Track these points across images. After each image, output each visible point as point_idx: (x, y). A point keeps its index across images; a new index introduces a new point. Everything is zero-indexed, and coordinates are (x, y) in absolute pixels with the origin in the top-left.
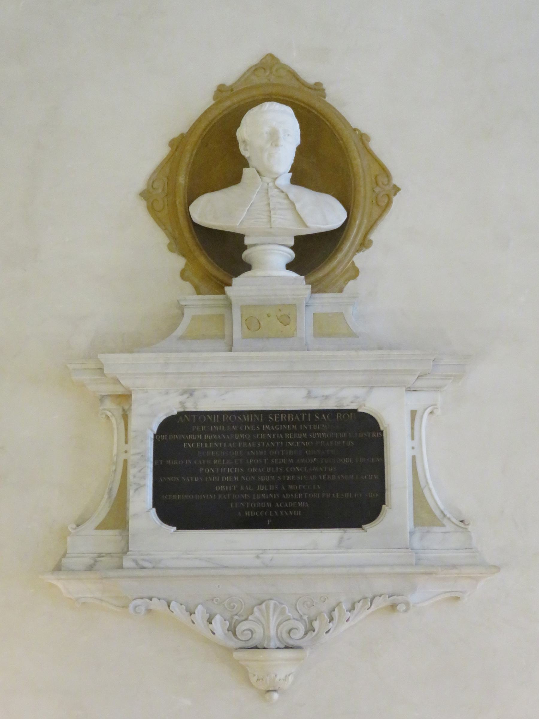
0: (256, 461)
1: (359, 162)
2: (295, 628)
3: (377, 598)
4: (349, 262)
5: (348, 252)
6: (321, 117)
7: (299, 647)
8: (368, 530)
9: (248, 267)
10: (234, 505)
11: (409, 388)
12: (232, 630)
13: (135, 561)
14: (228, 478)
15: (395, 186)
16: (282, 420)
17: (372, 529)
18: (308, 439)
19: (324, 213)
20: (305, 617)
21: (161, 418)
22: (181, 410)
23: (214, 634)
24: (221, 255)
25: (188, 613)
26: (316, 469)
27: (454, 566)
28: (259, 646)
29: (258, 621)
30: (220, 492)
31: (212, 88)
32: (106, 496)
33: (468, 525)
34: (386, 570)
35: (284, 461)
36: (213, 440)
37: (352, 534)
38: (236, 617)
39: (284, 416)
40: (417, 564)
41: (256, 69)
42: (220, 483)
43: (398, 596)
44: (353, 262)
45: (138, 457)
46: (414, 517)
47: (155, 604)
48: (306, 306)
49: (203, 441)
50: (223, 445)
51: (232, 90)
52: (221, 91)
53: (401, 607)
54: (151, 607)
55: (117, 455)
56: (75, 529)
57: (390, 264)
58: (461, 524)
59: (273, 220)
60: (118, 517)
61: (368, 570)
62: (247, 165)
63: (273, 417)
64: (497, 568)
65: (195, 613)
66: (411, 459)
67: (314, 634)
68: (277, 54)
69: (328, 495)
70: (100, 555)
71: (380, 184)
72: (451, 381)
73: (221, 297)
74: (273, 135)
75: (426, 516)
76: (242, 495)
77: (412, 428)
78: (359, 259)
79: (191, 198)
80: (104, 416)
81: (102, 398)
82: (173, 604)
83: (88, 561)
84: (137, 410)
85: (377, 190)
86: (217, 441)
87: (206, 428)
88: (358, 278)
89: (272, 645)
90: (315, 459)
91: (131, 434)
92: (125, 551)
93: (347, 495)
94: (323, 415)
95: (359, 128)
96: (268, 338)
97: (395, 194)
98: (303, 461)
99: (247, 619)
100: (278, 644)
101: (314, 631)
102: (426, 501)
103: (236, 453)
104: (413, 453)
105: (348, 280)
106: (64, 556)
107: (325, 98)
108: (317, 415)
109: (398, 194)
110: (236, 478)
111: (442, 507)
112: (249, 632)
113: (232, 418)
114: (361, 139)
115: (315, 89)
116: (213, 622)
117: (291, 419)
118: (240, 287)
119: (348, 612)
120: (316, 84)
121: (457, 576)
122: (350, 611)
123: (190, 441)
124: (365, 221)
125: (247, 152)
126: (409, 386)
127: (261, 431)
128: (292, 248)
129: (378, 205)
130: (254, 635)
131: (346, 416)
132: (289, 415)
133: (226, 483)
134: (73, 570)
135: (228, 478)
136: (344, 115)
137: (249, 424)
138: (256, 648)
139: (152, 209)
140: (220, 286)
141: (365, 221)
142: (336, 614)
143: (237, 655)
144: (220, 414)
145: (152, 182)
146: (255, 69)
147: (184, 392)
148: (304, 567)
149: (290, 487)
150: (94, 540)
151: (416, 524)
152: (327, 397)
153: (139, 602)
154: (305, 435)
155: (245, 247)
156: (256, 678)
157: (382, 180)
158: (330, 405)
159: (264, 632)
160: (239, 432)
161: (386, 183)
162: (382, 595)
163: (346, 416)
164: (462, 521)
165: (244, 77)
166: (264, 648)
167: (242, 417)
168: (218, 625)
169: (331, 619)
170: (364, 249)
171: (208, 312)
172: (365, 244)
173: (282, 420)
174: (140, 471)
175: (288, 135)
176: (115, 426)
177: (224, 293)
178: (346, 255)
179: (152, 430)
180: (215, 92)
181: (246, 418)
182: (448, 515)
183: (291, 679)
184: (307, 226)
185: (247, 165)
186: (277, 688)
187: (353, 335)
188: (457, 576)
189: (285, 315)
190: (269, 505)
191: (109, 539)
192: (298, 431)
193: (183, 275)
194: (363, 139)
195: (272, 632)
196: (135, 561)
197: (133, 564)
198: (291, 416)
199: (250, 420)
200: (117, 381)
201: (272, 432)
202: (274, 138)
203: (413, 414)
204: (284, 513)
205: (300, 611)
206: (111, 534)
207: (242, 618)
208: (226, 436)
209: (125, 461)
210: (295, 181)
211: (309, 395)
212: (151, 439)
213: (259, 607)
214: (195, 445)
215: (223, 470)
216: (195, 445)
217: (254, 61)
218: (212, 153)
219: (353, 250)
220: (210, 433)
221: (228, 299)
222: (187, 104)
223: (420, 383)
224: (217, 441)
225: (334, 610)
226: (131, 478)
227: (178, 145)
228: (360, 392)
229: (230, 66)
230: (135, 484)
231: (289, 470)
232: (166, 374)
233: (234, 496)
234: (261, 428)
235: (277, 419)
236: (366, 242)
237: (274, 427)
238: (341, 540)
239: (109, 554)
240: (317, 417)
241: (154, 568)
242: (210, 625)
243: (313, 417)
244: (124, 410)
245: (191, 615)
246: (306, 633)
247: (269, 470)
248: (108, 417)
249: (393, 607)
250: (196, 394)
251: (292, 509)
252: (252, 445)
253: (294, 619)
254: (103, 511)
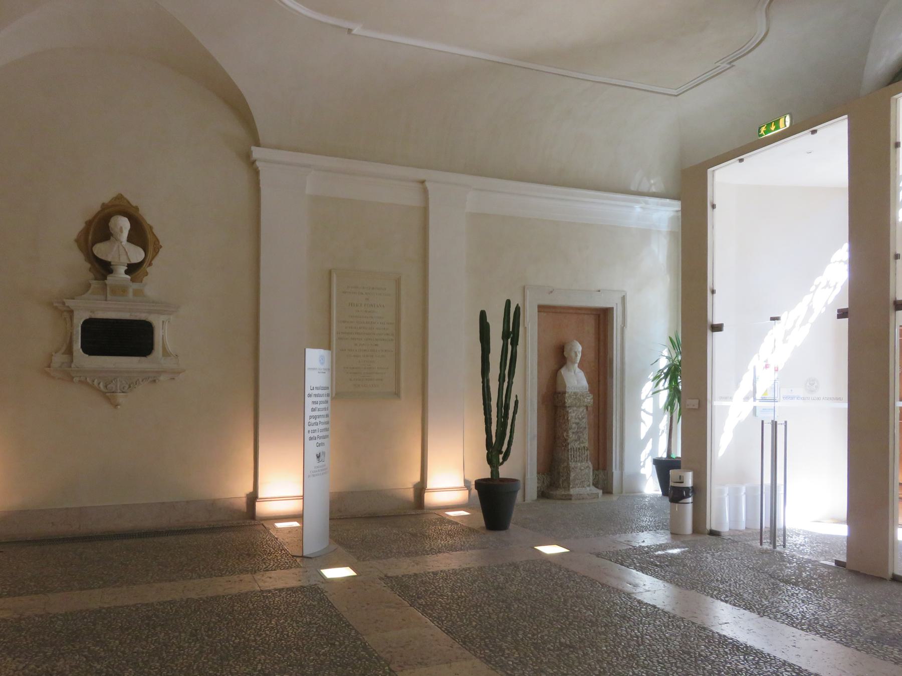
1: (149, 236)
12: (106, 386)
17: (150, 357)
19: (136, 255)
24: (104, 268)
60: (69, 351)
75: (166, 354)
78: (148, 269)
79: (93, 244)
92: (72, 361)
118: (110, 279)
140: (105, 278)
150: (59, 359)
168: (101, 385)
194: (151, 228)
217: (115, 196)
218: (99, 229)
221: (106, 285)
229: (106, 196)
254: (64, 348)
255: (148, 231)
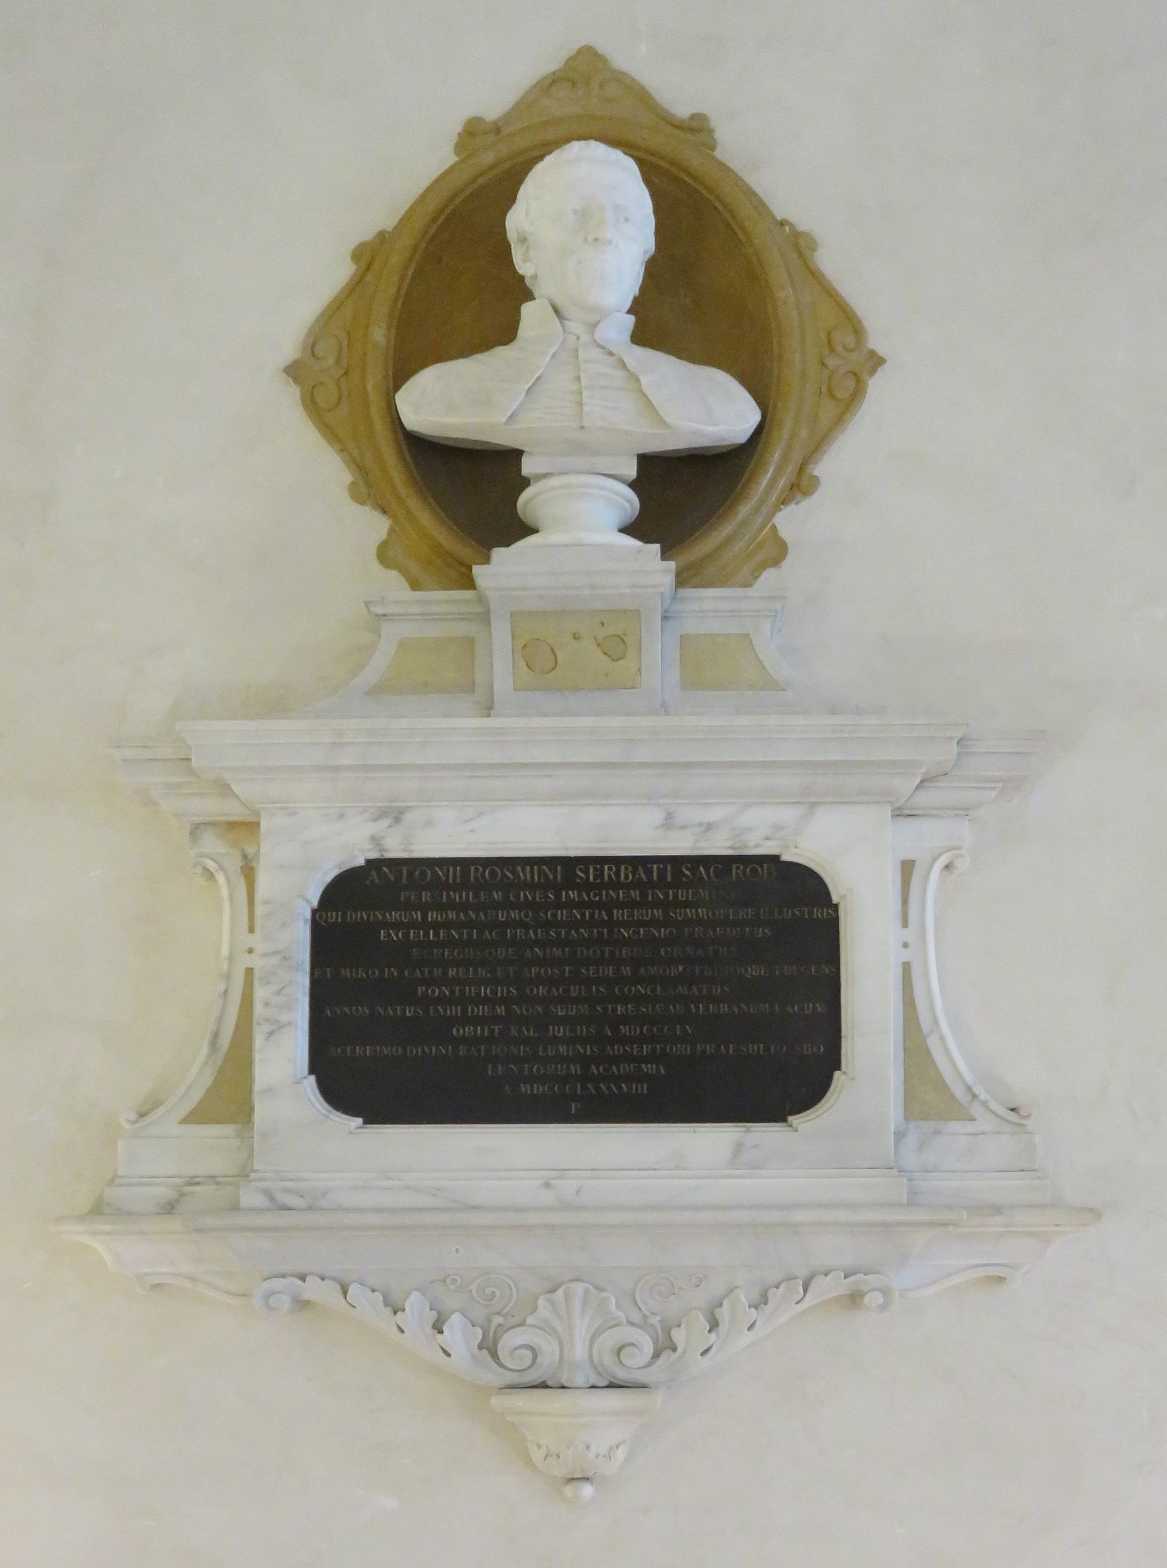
0: (546, 971)
1: (788, 297)
2: (633, 1344)
3: (819, 1279)
4: (764, 526)
5: (762, 502)
6: (704, 192)
7: (643, 1386)
8: (800, 1127)
9: (526, 530)
10: (495, 1069)
11: (900, 809)
12: (490, 1347)
13: (268, 1194)
14: (482, 1010)
15: (872, 354)
16: (606, 878)
18: (666, 922)
19: (709, 408)
20: (655, 1320)
21: (329, 874)
22: (374, 855)
23: (448, 1355)
24: (470, 494)
25: (388, 1310)
26: (682, 990)
27: (997, 1210)
28: (550, 1383)
29: (545, 1328)
30: (465, 1040)
31: (454, 127)
32: (205, 1049)
33: (1029, 1116)
34: (843, 1215)
35: (610, 971)
36: (448, 925)
37: (764, 1134)
38: (497, 1320)
39: (610, 869)
40: (909, 1204)
41: (554, 82)
42: (464, 1020)
43: (865, 1274)
44: (774, 528)
45: (275, 960)
46: (906, 1099)
47: (312, 1290)
48: (665, 618)
49: (425, 925)
50: (470, 935)
51: (498, 131)
52: (473, 133)
53: (874, 1299)
54: (307, 1296)
55: (231, 959)
56: (135, 1122)
57: (860, 520)
58: (1013, 1117)
59: (586, 409)
60: (229, 1097)
61: (799, 1216)
62: (529, 296)
63: (587, 873)
64: (1095, 1213)
65: (403, 1310)
66: (900, 970)
67: (675, 1356)
68: (604, 46)
69: (710, 1049)
70: (193, 1182)
71: (839, 348)
72: (994, 794)
73: (468, 594)
74: (588, 229)
75: (928, 1094)
76: (512, 1047)
77: (905, 901)
78: (790, 522)
80: (199, 870)
81: (196, 830)
82: (353, 1289)
83: (163, 1192)
84: (272, 853)
85: (832, 362)
86: (459, 925)
87: (432, 897)
88: (785, 564)
89: (580, 1380)
90: (680, 968)
91: (259, 910)
93: (754, 1049)
94: (701, 869)
95: (793, 219)
96: (576, 689)
97: (873, 372)
98: (653, 970)
99: (522, 1324)
100: (594, 1380)
101: (674, 1349)
102: (933, 1062)
103: (501, 953)
104: (906, 955)
105: (762, 567)
106: (111, 1182)
107: (713, 149)
108: (687, 869)
109: (879, 373)
110: (500, 1010)
111: (969, 1078)
112: (529, 1353)
113: (493, 873)
114: (796, 246)
115: (691, 130)
116: (445, 1329)
117: (626, 877)
118: (506, 570)
119: (753, 1310)
120: (693, 117)
121: (1003, 1229)
122: (756, 1308)
123: (397, 926)
124: (804, 433)
125: (528, 264)
126: (898, 805)
127: (559, 905)
128: (633, 485)
129: (833, 397)
130: (539, 1359)
131: (754, 871)
132: (623, 868)
133: (477, 1020)
134: (129, 1214)
135: (482, 1010)
136: (759, 190)
137: (531, 886)
138: (543, 1386)
139: (312, 405)
141: (804, 433)
142: (724, 1314)
143: (495, 1401)
144: (464, 863)
145: (312, 344)
146: (551, 83)
147: (382, 814)
148: (653, 1208)
149: (624, 1030)
151: (909, 1115)
152: (709, 827)
153: (278, 1283)
154: (658, 913)
155: (525, 483)
156: (542, 1453)
157: (844, 338)
158: (718, 845)
159: (561, 1350)
160: (507, 905)
161: (852, 345)
162: (831, 1271)
163: (754, 871)
164: (1013, 1110)
165: (526, 104)
166: (563, 1387)
167: (514, 872)
169: (714, 1325)
170: (799, 497)
171: (435, 631)
172: (800, 486)
173: (606, 878)
174: (279, 993)
175: (626, 220)
176: (225, 892)
177: (469, 583)
178: (757, 509)
179: (307, 901)
180: (459, 135)
181: (524, 874)
182: (983, 1096)
183: (621, 1454)
184: (666, 425)
185: (529, 296)
186: (589, 1474)
187: (772, 685)
188: (1003, 1229)
189: (615, 634)
190: (575, 1069)
191: (210, 1149)
192: (641, 904)
193: (384, 555)
194: (800, 245)
195: (579, 1351)
196: (268, 1194)
197: (260, 1201)
198: (626, 869)
199: (532, 877)
200: (224, 789)
201: (581, 905)
202: (587, 222)
203: (907, 868)
204: (609, 1088)
205: (642, 1306)
206: (217, 1136)
207: (514, 1321)
208: (477, 915)
209: (249, 972)
210: (640, 337)
211: (669, 823)
212: (305, 921)
213: (548, 1296)
214: (406, 935)
215: (470, 990)
216: (406, 935)
217: (551, 64)
218: (452, 272)
219: (773, 498)
220: (441, 908)
222: (400, 168)
223: (925, 798)
224: (459, 925)
225: (721, 1305)
226: (258, 1008)
227: (368, 256)
228: (788, 815)
229: (494, 82)
230: (267, 1020)
231: (621, 990)
232: (337, 769)
233: (495, 1050)
234: (558, 896)
235: (595, 877)
236: (804, 482)
237: (588, 895)
238: (739, 1148)
239: (213, 1179)
240: (687, 872)
241: (310, 1208)
242: (439, 1336)
243: (677, 873)
244: (245, 857)
245: (395, 1313)
246: (656, 1355)
247: (574, 991)
248: (210, 875)
249: (854, 1299)
250: (408, 817)
251: (627, 1078)
252: (536, 934)
253: (631, 1323)
255: (779, 275)
